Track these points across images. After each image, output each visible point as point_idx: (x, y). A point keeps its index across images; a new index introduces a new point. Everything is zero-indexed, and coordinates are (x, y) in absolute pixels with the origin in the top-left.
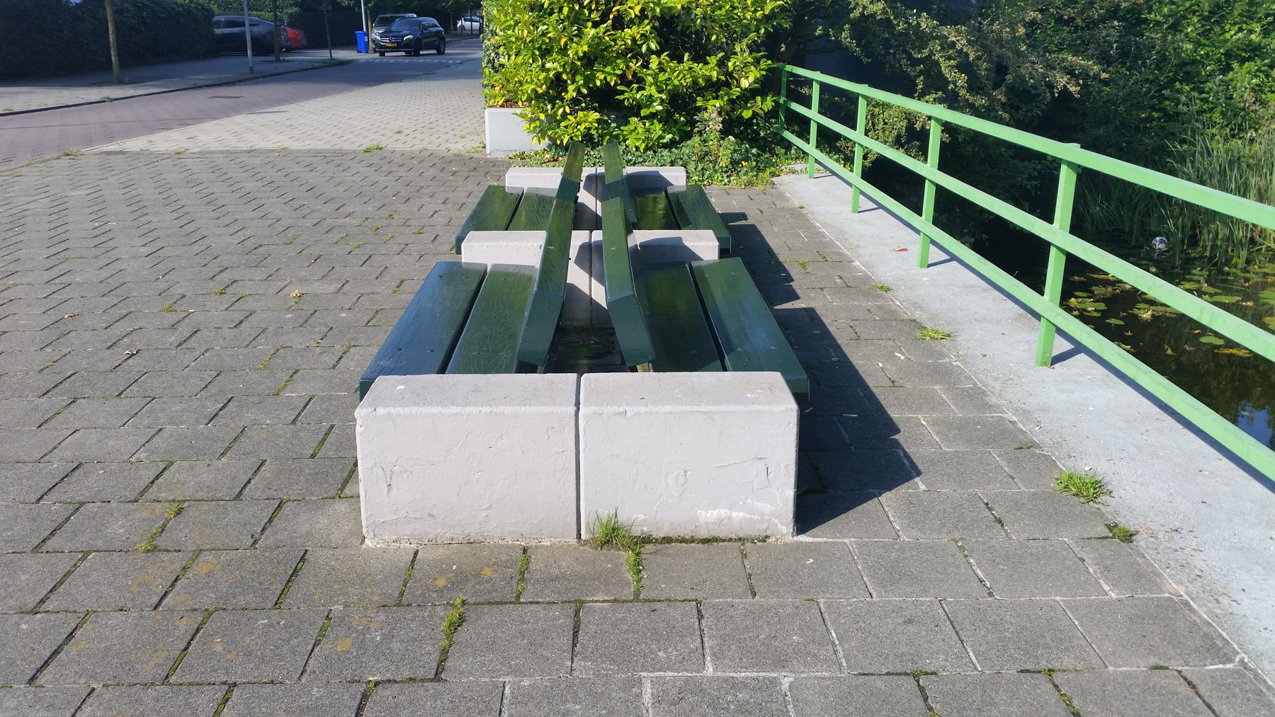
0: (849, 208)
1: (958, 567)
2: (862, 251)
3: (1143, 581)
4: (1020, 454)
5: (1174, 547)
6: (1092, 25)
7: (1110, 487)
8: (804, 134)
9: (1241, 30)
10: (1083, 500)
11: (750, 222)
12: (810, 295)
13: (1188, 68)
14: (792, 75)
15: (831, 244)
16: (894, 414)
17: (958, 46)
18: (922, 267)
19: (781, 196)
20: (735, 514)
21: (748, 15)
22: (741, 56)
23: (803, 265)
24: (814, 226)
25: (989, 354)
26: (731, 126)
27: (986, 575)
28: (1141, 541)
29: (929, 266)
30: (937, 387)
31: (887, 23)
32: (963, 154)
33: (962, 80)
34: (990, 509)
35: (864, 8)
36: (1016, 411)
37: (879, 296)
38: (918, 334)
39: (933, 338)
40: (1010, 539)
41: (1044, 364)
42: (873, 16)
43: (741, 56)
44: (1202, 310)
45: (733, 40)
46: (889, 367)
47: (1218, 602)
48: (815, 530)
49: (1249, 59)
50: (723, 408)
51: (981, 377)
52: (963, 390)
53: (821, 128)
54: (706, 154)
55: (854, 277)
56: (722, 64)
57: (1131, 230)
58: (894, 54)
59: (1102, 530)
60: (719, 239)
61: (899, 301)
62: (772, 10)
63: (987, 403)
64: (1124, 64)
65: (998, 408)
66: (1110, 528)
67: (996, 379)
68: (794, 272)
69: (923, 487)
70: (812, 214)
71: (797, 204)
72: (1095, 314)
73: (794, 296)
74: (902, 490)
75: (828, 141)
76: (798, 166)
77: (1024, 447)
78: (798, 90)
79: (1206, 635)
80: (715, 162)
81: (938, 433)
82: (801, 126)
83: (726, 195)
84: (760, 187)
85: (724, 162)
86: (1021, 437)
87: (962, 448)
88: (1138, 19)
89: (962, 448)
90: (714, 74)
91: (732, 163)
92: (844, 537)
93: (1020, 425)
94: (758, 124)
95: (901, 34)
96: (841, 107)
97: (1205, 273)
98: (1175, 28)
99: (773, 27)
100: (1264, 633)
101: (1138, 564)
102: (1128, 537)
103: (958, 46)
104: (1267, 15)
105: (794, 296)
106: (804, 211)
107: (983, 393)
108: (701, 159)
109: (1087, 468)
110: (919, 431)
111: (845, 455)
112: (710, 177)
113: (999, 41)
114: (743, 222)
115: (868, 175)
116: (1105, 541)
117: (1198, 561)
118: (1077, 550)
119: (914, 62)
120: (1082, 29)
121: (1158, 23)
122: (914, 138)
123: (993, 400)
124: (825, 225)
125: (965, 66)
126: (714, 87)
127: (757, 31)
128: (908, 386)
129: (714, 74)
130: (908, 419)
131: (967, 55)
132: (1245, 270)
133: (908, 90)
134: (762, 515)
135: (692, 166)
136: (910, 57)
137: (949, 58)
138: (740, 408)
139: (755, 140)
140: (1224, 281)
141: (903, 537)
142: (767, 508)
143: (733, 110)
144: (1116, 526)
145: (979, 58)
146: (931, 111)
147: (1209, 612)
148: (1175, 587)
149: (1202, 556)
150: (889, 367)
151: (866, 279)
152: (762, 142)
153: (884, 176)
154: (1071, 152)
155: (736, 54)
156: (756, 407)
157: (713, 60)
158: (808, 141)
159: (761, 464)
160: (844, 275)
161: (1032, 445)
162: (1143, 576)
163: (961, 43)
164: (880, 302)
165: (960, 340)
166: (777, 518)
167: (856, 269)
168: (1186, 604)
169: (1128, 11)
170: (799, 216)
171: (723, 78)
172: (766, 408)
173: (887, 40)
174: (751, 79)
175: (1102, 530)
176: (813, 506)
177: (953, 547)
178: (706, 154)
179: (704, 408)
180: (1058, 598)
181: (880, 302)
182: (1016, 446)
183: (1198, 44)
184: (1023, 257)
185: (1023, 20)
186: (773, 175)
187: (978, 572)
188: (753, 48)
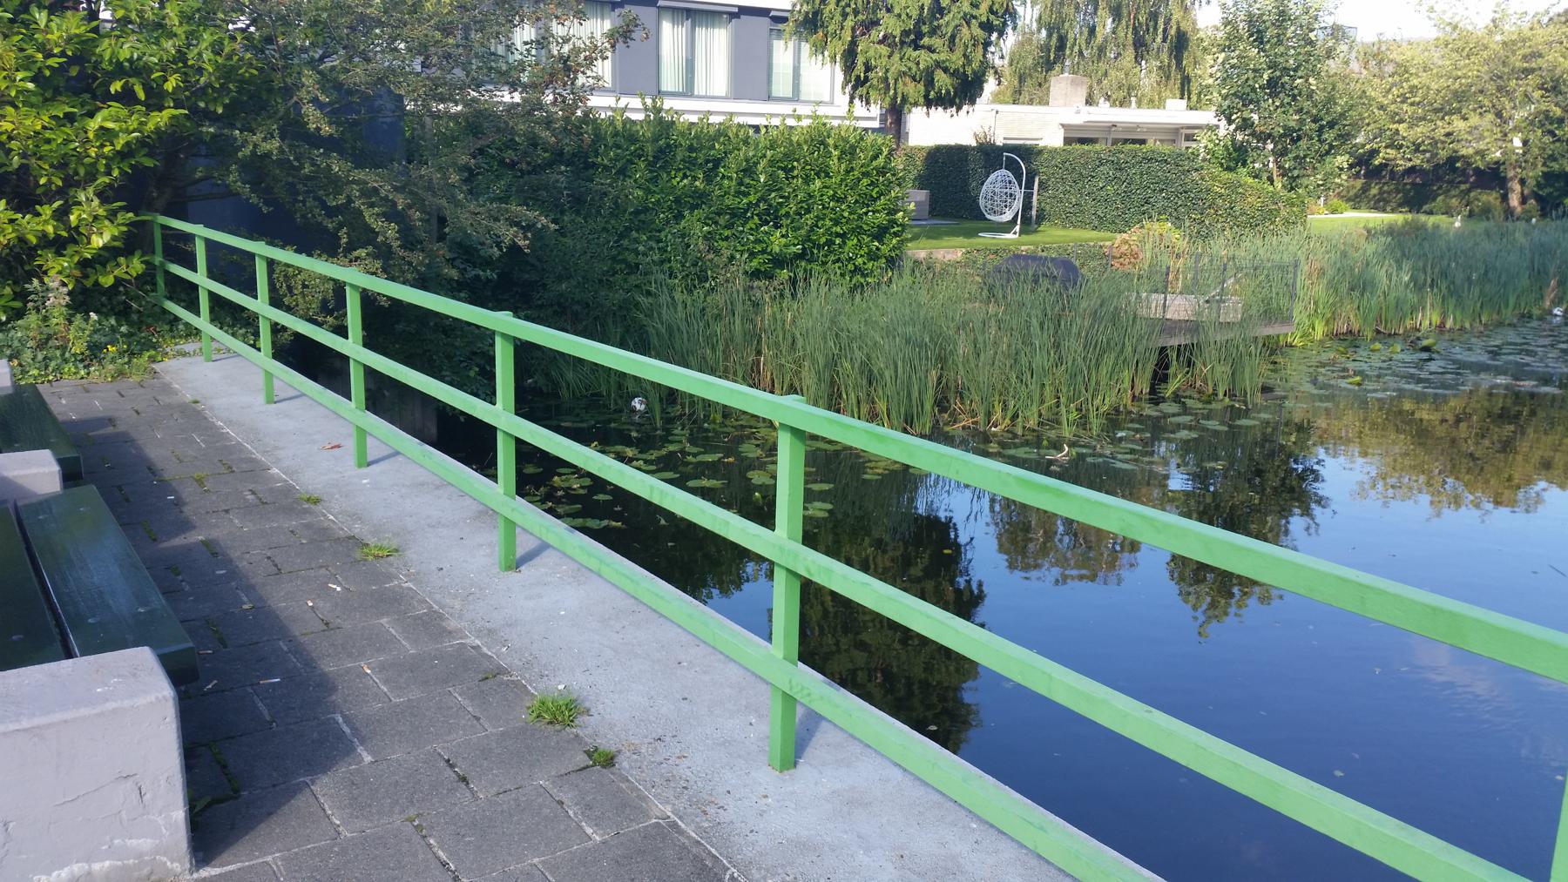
0: (261, 399)
1: (415, 855)
2: (281, 453)
3: (628, 811)
4: (485, 686)
5: (658, 759)
6: (536, 169)
7: (587, 704)
8: (193, 307)
9: (685, 176)
10: (558, 727)
11: (121, 428)
12: (218, 524)
13: (642, 217)
14: (164, 227)
15: (239, 448)
16: (329, 667)
17: (383, 193)
18: (360, 466)
19: (167, 389)
20: (96, 867)
21: (93, 152)
22: (87, 205)
23: (200, 482)
24: (213, 426)
25: (446, 566)
26: (83, 300)
27: (451, 854)
28: (624, 763)
29: (369, 464)
30: (384, 621)
31: (283, 163)
32: (388, 326)
33: (391, 232)
34: (452, 766)
35: (255, 146)
36: (478, 633)
37: (306, 511)
38: (358, 555)
39: (377, 557)
40: (477, 799)
41: (509, 568)
42: (268, 155)
43: (87, 205)
44: (652, 488)
45: (71, 183)
46: (321, 604)
47: (705, 813)
48: (225, 856)
49: (697, 207)
50: (58, 717)
51: (438, 597)
52: (420, 617)
53: (214, 297)
54: (49, 338)
55: (271, 490)
56: (61, 215)
57: (609, 395)
58: (304, 202)
59: (582, 760)
60: (61, 462)
61: (331, 516)
62: (128, 144)
63: (445, 630)
64: (578, 213)
65: (457, 633)
66: (589, 754)
67: (455, 597)
68: (188, 492)
69: (368, 758)
70: (211, 409)
71: (189, 397)
72: (582, 492)
73: (185, 526)
74: (343, 770)
75: (230, 316)
76: (189, 346)
77: (489, 678)
78: (179, 248)
79: (695, 857)
80: (64, 348)
81: (386, 682)
82: (187, 294)
83: (72, 395)
84: (135, 379)
85: (78, 347)
86: (486, 664)
87: (415, 694)
88: (586, 162)
89: (415, 694)
90: (50, 229)
91: (89, 348)
92: (266, 855)
93: (485, 650)
94: (126, 293)
95: (308, 178)
96: (235, 269)
97: (686, 432)
98: (622, 172)
99: (131, 166)
100: (752, 837)
101: (620, 790)
102: (609, 761)
103: (383, 193)
104: (708, 161)
105: (185, 526)
106: (200, 407)
107: (441, 617)
108: (42, 345)
109: (561, 687)
110: (366, 679)
111: (248, 738)
112: (58, 369)
113: (430, 188)
114: (110, 430)
115: (280, 354)
116: (584, 773)
117: (683, 770)
118: (554, 791)
119: (331, 212)
120: (529, 173)
121: (606, 168)
122: (331, 307)
123: (452, 624)
124: (229, 423)
125: (392, 215)
126: (57, 246)
127: (109, 173)
128: (347, 625)
129: (50, 229)
130: (348, 671)
131: (394, 204)
132: (723, 425)
133: (327, 246)
134: (140, 856)
135: (27, 356)
136: (324, 205)
137: (372, 205)
138: (84, 711)
139: (123, 313)
140: (707, 438)
141: (346, 833)
142: (145, 844)
143: (86, 276)
144: (596, 749)
145: (410, 207)
146: (356, 277)
147: (699, 829)
148: (662, 809)
149: (686, 762)
150: (321, 604)
151: (288, 490)
152: (135, 317)
153: (305, 357)
154: (504, 323)
155: (80, 204)
156: (110, 706)
157: (47, 211)
158: (198, 314)
159: (130, 783)
160: (258, 488)
161: (501, 671)
162: (628, 805)
163: (386, 190)
164: (308, 519)
165: (410, 554)
166: (165, 854)
167: (273, 478)
168: (674, 825)
169: (574, 155)
170: (193, 415)
171: (64, 234)
172: (127, 703)
173: (292, 185)
174: (107, 237)
175: (582, 760)
176: (211, 828)
177: (408, 829)
178: (49, 338)
179: (25, 724)
180: (536, 860)
181: (308, 519)
182: (481, 676)
183: (648, 191)
184: (468, 442)
185: (455, 164)
186: (153, 360)
187: (441, 853)
188: (102, 196)
